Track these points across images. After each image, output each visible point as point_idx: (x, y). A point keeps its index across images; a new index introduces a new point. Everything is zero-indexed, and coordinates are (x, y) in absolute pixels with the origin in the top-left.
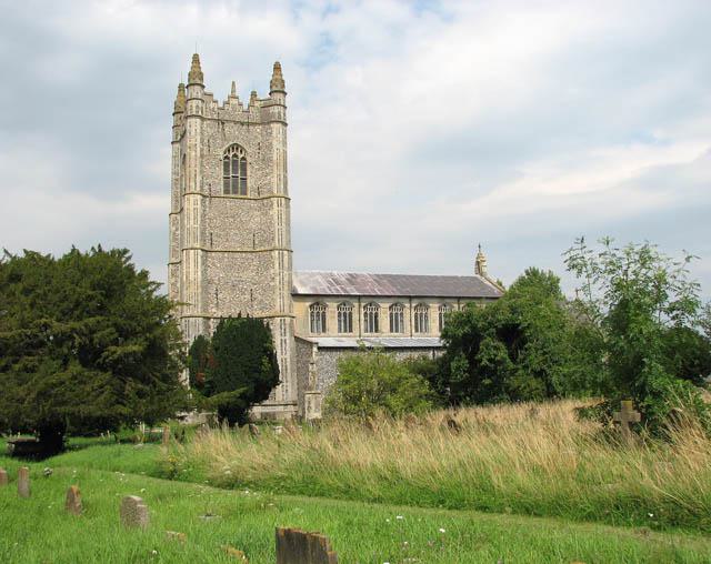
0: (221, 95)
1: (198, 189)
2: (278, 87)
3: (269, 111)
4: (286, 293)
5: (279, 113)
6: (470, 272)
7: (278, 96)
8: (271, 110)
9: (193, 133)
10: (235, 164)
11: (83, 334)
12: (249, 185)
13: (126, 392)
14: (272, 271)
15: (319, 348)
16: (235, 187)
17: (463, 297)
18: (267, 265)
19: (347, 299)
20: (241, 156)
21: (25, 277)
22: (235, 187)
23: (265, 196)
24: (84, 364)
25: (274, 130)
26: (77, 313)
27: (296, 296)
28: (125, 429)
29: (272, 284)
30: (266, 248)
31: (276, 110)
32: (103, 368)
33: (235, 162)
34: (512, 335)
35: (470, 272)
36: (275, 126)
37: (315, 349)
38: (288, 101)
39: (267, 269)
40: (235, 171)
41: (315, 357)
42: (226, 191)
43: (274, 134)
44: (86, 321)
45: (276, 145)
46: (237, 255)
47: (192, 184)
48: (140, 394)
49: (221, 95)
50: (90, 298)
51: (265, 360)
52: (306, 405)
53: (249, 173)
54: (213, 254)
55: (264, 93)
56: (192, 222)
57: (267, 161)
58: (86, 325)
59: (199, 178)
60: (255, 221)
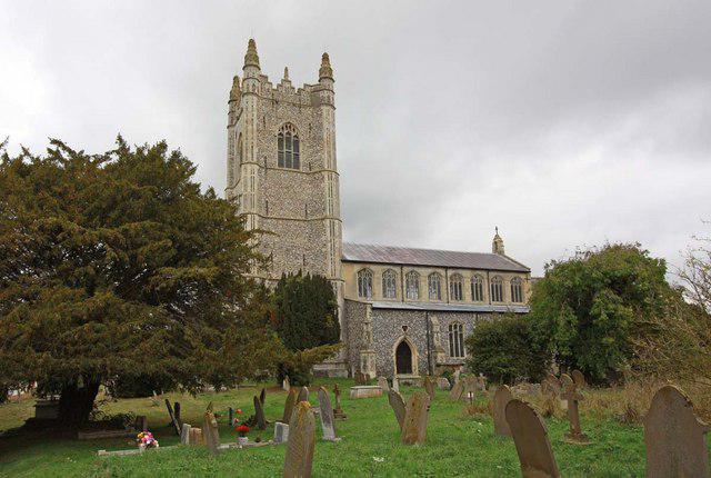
0: (275, 79)
1: (255, 160)
2: (326, 73)
3: (319, 97)
4: (338, 259)
5: (329, 97)
6: (489, 250)
7: (326, 82)
8: (321, 94)
9: (250, 110)
10: (288, 143)
11: (120, 246)
12: (301, 161)
13: (186, 337)
14: (323, 238)
15: (373, 309)
16: (288, 160)
17: (493, 270)
18: (318, 233)
19: (391, 267)
20: (293, 134)
21: (53, 181)
22: (288, 160)
23: (317, 170)
24: (125, 292)
25: (324, 111)
26: (113, 215)
27: (344, 261)
28: (265, 262)
29: (324, 250)
30: (319, 217)
31: (325, 94)
32: (151, 300)
33: (288, 140)
34: (620, 284)
35: (489, 250)
36: (324, 108)
37: (369, 310)
38: (336, 87)
39: (319, 236)
40: (288, 147)
41: (369, 318)
42: (281, 164)
43: (325, 115)
44: (126, 226)
45: (326, 125)
46: (290, 223)
47: (249, 155)
48: (208, 342)
49: (275, 79)
50: (135, 195)
51: (329, 317)
52: (362, 364)
53: (301, 149)
54: (269, 221)
55: (314, 80)
56: (249, 189)
57: (317, 140)
58: (125, 232)
59: (256, 150)
60: (306, 193)
